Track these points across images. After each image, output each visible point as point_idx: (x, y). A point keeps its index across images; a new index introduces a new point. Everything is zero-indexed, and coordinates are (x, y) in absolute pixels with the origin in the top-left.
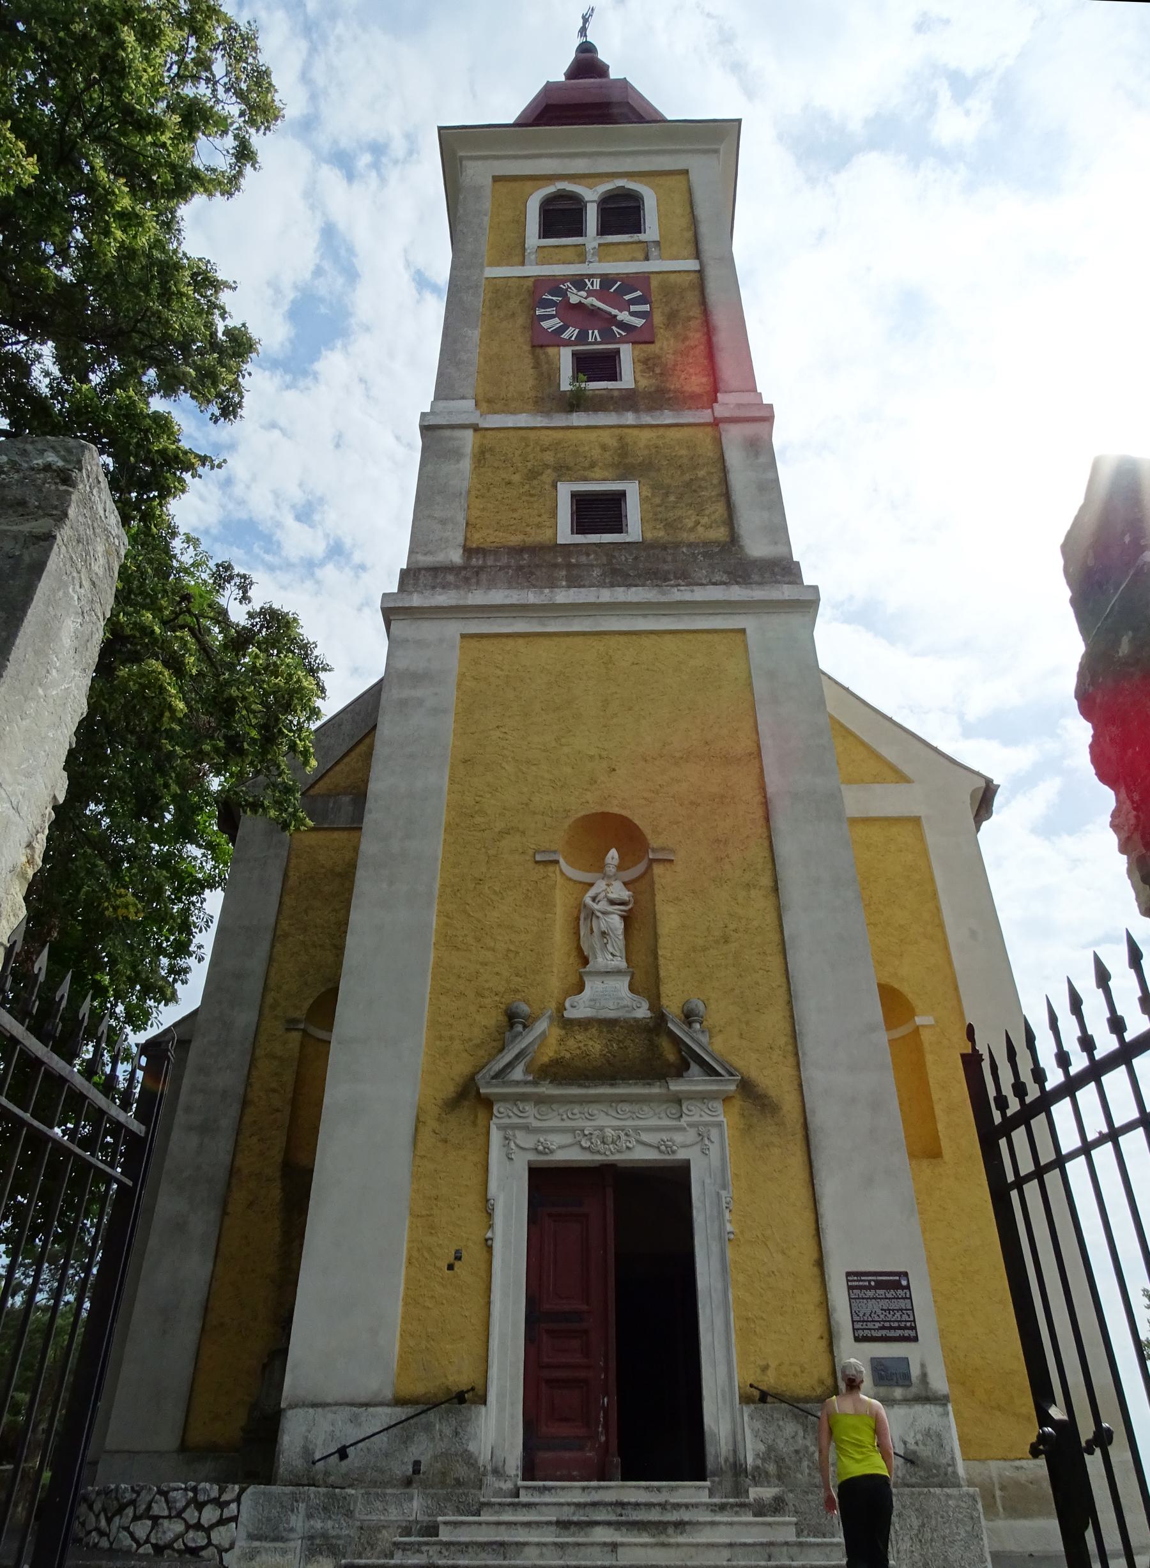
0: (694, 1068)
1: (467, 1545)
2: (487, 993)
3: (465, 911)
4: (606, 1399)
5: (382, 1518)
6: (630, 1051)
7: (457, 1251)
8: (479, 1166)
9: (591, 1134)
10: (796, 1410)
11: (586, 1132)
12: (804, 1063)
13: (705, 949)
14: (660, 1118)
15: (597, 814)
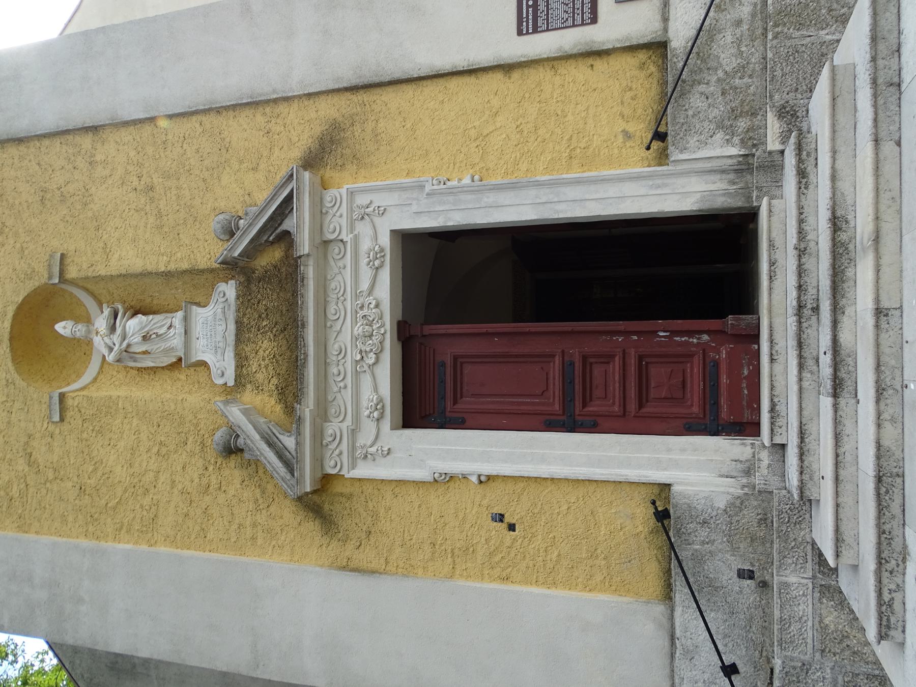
0: (287, 226)
1: (881, 532)
2: (205, 481)
3: (114, 508)
4: (661, 334)
5: (810, 623)
6: (270, 305)
7: (494, 519)
8: (397, 490)
9: (361, 352)
10: (675, 95)
11: (359, 357)
12: (284, 92)
13: (159, 215)
14: (345, 267)
15: (12, 349)
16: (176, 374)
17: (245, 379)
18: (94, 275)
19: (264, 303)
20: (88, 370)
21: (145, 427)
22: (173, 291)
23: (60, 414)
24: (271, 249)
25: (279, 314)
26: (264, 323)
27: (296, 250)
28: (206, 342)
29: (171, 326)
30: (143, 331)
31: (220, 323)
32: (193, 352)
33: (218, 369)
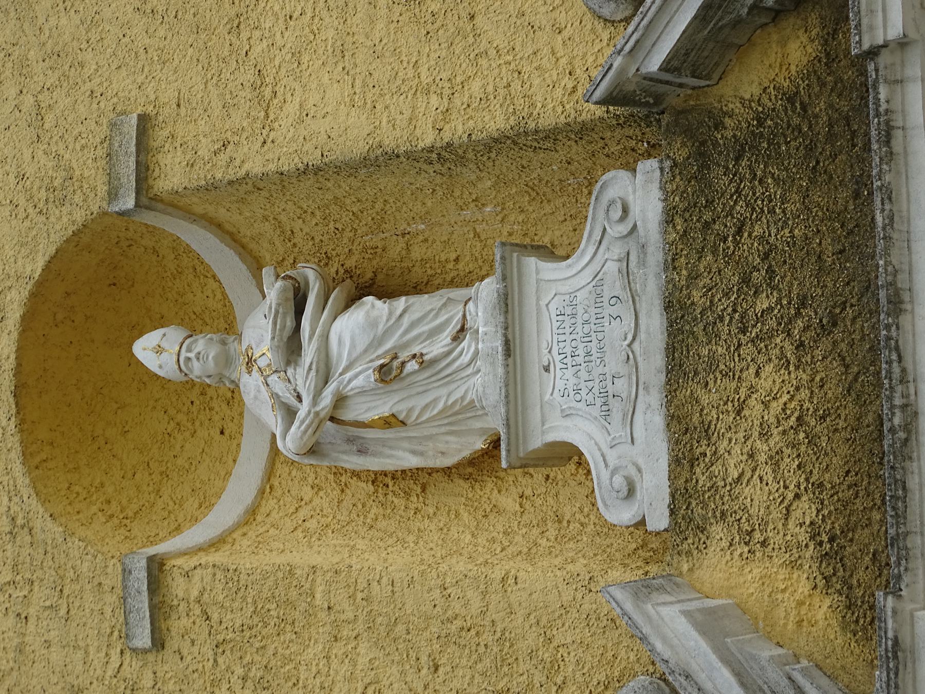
6: (779, 237)
16: (488, 491)
17: (705, 506)
18: (231, 175)
19: (758, 230)
20: (232, 484)
21: (395, 669)
22: (467, 214)
23: (152, 624)
24: (775, 37)
25: (812, 266)
26: (763, 304)
27: (858, 26)
28: (573, 380)
29: (462, 329)
30: (380, 351)
31: (614, 311)
32: (535, 416)
33: (613, 474)
